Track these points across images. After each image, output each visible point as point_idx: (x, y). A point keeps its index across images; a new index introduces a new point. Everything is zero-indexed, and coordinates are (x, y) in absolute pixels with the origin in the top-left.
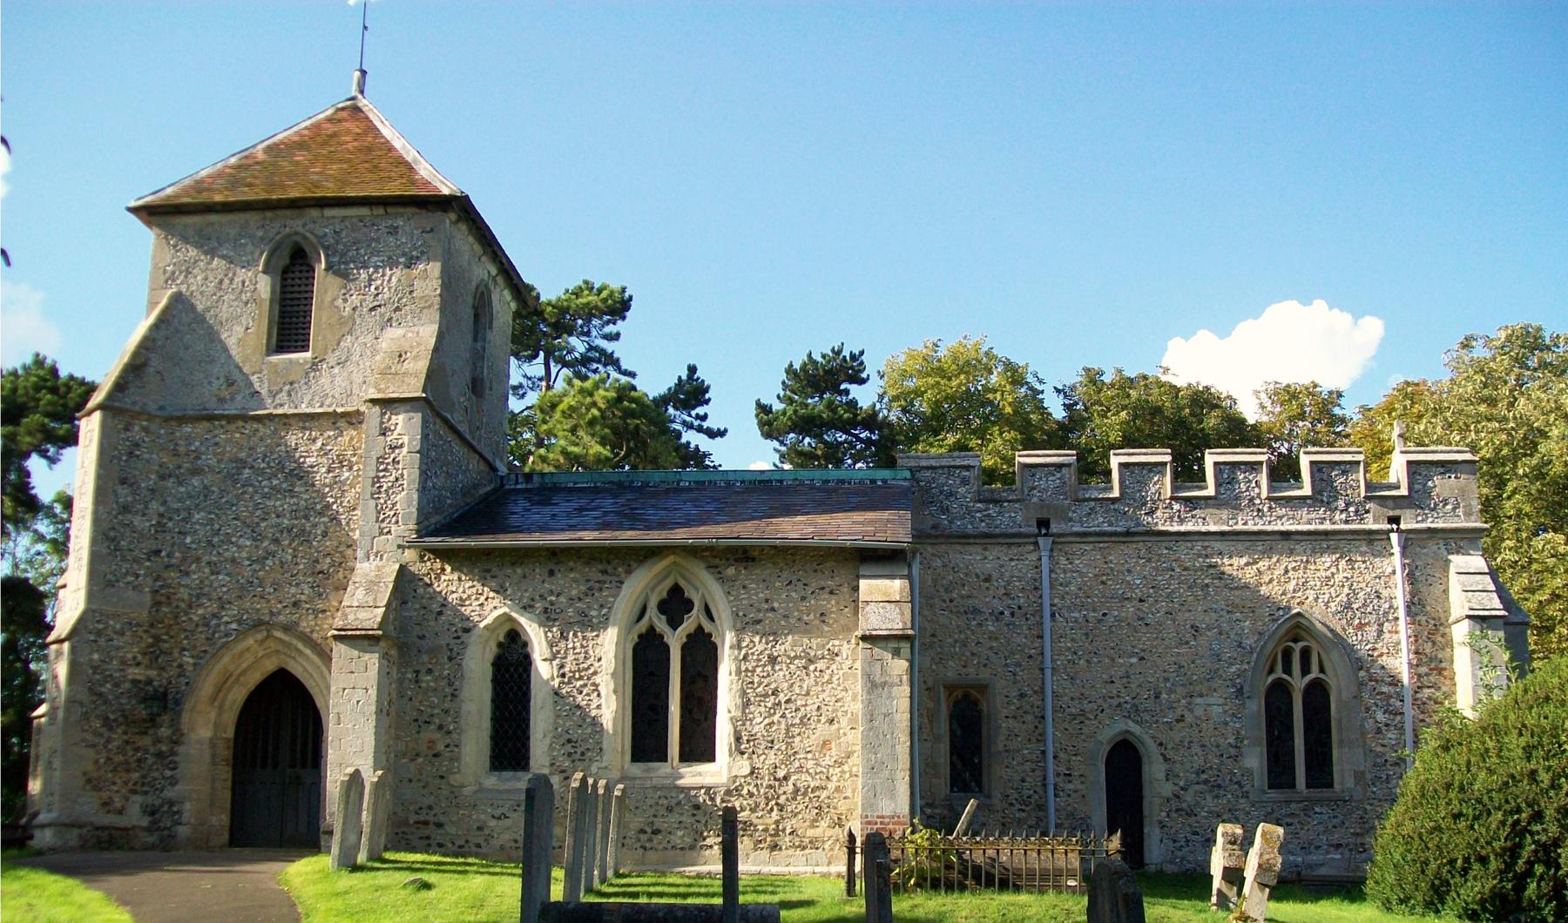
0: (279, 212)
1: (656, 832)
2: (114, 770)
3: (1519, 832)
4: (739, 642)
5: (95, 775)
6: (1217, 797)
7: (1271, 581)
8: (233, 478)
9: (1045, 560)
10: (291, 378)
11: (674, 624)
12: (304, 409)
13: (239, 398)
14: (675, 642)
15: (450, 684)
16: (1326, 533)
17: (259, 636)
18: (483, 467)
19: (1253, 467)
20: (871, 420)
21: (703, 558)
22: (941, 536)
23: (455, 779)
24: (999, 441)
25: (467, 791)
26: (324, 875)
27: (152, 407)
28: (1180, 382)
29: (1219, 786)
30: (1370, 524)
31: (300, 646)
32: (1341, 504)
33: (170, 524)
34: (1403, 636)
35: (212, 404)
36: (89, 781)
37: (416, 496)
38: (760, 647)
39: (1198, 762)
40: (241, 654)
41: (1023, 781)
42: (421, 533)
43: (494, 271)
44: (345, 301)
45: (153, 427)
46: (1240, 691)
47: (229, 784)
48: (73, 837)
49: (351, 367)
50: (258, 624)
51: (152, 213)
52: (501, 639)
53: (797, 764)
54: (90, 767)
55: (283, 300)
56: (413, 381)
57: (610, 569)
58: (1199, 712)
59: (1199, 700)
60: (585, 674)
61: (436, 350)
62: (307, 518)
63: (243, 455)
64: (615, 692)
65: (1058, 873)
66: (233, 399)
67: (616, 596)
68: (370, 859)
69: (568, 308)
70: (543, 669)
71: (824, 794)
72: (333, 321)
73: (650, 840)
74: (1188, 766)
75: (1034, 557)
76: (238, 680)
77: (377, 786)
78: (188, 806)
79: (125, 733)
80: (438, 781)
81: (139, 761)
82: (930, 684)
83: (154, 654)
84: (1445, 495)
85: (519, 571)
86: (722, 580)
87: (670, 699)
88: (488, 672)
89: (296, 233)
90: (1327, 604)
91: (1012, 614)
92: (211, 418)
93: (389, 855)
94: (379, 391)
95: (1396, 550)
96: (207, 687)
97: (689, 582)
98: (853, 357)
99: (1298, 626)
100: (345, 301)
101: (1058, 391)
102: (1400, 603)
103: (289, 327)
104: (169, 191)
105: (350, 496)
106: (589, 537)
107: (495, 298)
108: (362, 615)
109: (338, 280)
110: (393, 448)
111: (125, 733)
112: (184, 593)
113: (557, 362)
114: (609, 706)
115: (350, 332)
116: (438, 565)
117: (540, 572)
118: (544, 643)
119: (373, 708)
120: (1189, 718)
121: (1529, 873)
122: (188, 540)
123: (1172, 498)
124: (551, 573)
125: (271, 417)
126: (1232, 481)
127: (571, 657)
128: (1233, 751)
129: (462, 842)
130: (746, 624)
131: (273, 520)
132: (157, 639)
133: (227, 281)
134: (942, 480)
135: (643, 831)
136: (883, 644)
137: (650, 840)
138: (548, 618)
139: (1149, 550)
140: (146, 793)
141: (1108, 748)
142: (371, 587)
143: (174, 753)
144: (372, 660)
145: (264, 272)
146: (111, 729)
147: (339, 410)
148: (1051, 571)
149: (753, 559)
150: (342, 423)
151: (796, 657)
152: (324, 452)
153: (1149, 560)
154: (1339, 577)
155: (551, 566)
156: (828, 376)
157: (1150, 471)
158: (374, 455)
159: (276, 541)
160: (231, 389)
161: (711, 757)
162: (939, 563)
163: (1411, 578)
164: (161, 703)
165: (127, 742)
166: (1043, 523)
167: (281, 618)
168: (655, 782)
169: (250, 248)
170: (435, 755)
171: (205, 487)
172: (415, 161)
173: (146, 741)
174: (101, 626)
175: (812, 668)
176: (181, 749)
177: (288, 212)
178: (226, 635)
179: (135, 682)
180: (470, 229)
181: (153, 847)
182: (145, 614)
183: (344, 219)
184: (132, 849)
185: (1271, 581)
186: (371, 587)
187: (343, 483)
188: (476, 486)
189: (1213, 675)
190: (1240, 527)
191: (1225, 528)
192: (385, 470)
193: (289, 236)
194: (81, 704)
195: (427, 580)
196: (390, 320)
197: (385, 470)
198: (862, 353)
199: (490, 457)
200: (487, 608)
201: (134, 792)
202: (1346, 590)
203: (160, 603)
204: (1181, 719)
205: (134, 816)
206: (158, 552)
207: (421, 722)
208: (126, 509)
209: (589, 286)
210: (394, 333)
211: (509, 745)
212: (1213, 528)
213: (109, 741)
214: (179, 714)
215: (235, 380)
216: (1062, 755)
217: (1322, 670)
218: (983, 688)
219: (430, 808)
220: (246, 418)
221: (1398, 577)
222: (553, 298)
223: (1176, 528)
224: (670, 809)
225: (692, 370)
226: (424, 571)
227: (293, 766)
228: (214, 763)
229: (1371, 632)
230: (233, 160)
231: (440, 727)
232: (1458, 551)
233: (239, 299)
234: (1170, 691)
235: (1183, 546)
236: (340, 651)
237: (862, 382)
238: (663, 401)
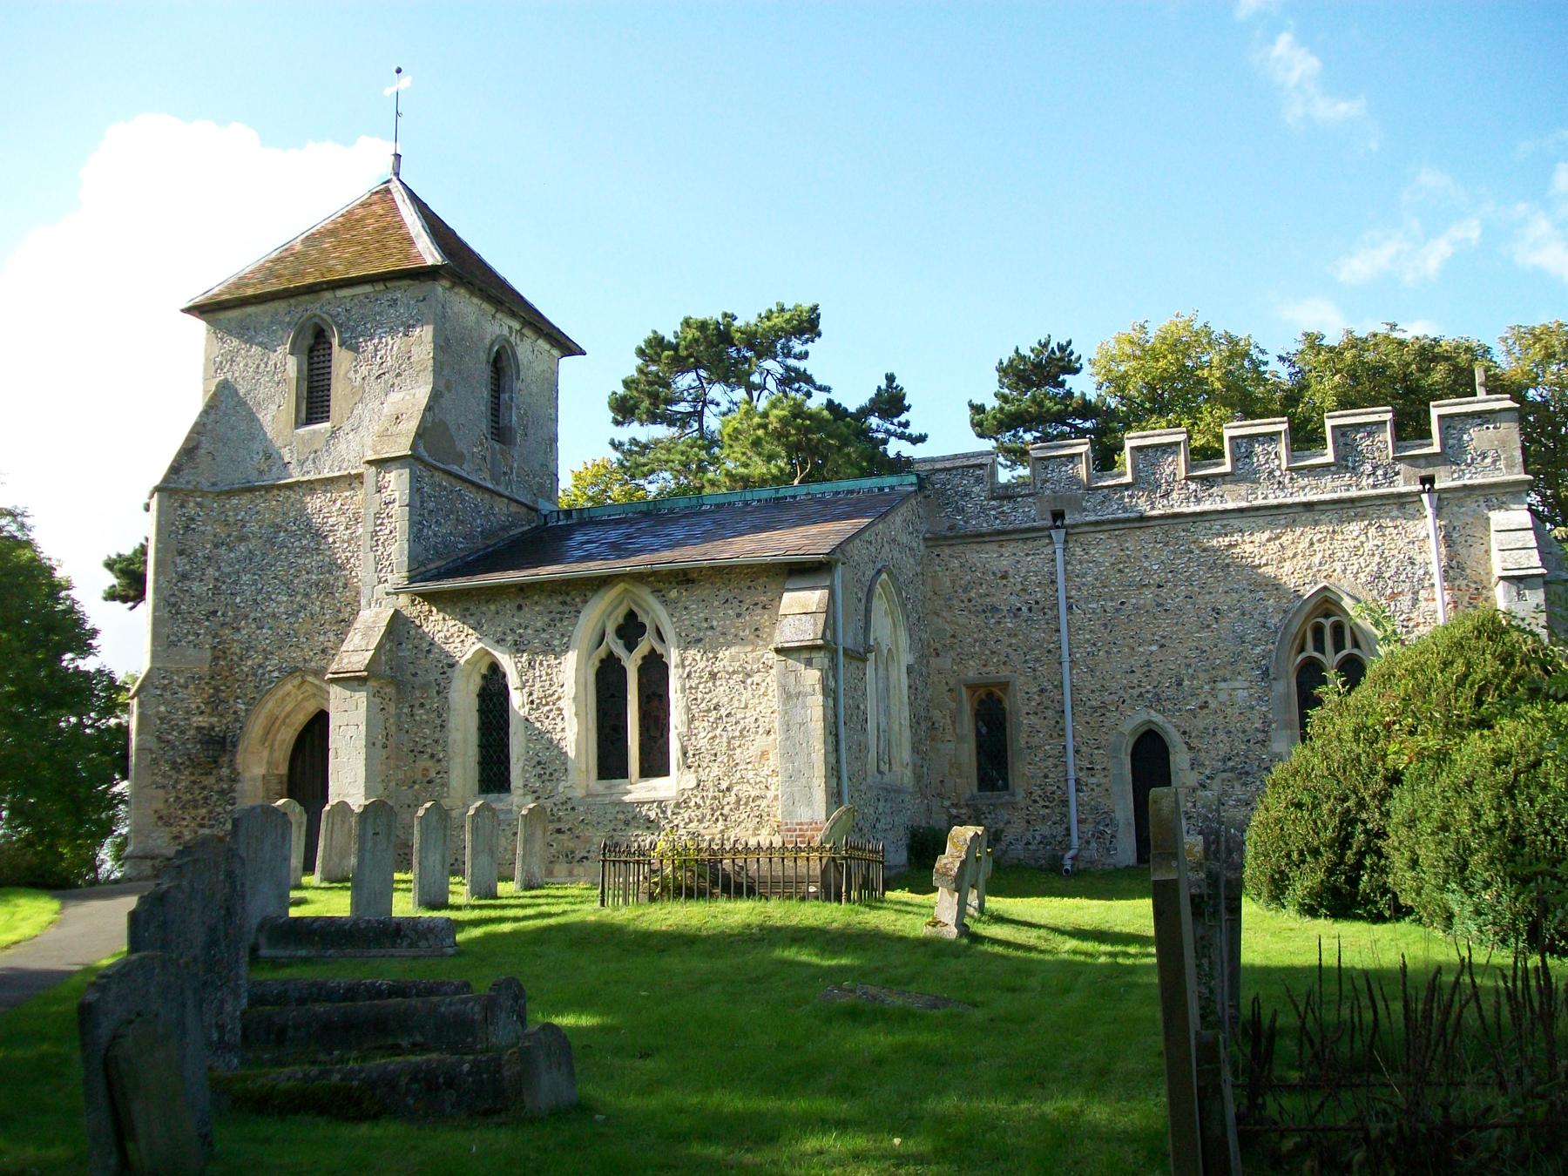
2: (183, 807)
3: (1348, 820)
4: (683, 660)
6: (1245, 784)
7: (1295, 555)
8: (270, 541)
9: (1059, 553)
12: (326, 474)
16: (1352, 500)
17: (296, 682)
19: (1272, 437)
20: (1086, 409)
21: (648, 583)
22: (956, 537)
24: (1209, 419)
27: (205, 485)
28: (1408, 337)
29: (1247, 773)
30: (1400, 487)
32: (1368, 468)
34: (1439, 604)
35: (254, 476)
36: (160, 818)
38: (702, 665)
39: (1224, 749)
40: (283, 699)
41: (1046, 777)
42: (412, 580)
44: (356, 372)
45: (207, 502)
46: (1266, 673)
49: (362, 431)
52: (484, 671)
53: (738, 775)
54: (160, 805)
57: (568, 599)
58: (1223, 697)
59: (1222, 685)
62: (330, 572)
63: (278, 520)
65: (799, 881)
70: (517, 699)
71: (764, 803)
74: (1213, 754)
75: (1049, 550)
79: (192, 774)
81: (206, 798)
82: (951, 686)
83: (215, 703)
84: (1485, 447)
85: (493, 607)
86: (665, 603)
87: (631, 717)
88: (474, 703)
90: (1356, 576)
91: (1030, 610)
92: (252, 490)
94: (376, 452)
95: (1429, 512)
96: (256, 729)
98: (1061, 348)
99: (1326, 600)
100: (356, 372)
101: (1281, 358)
102: (1434, 569)
103: (315, 403)
104: (216, 291)
111: (192, 774)
112: (236, 648)
114: (572, 731)
115: (361, 401)
116: (426, 608)
117: (510, 606)
120: (1213, 704)
121: (1359, 865)
123: (1187, 478)
124: (520, 608)
126: (1249, 455)
127: (538, 685)
128: (1260, 736)
130: (687, 643)
132: (217, 689)
134: (956, 481)
136: (796, 656)
138: (518, 648)
139: (1166, 533)
140: (212, 826)
141: (1132, 741)
143: (233, 791)
144: (361, 698)
146: (179, 771)
148: (1067, 563)
149: (693, 581)
151: (734, 672)
153: (1166, 544)
154: (1368, 546)
156: (1040, 371)
157: (1164, 452)
158: (372, 511)
159: (307, 595)
161: (665, 772)
162: (956, 563)
163: (1449, 541)
164: (218, 747)
165: (194, 782)
166: (1058, 515)
170: (429, 782)
175: (749, 681)
176: (238, 786)
177: (307, 297)
179: (199, 729)
182: (206, 667)
185: (1295, 555)
189: (1237, 657)
190: (1260, 502)
191: (1244, 504)
193: (310, 318)
194: (151, 751)
198: (1069, 343)
200: (467, 644)
202: (1377, 559)
204: (1205, 706)
207: (417, 752)
208: (184, 577)
210: (395, 397)
211: (494, 775)
212: (1230, 505)
213: (176, 782)
214: (234, 754)
216: (1084, 749)
217: (1356, 644)
218: (1005, 686)
220: (280, 487)
221: (1432, 542)
223: (1193, 508)
224: (627, 823)
225: (890, 378)
229: (1405, 601)
230: (274, 255)
231: (432, 756)
232: (1501, 506)
233: (273, 375)
234: (1193, 677)
235: (1201, 526)
236: (335, 690)
237: (1076, 371)
238: (864, 412)
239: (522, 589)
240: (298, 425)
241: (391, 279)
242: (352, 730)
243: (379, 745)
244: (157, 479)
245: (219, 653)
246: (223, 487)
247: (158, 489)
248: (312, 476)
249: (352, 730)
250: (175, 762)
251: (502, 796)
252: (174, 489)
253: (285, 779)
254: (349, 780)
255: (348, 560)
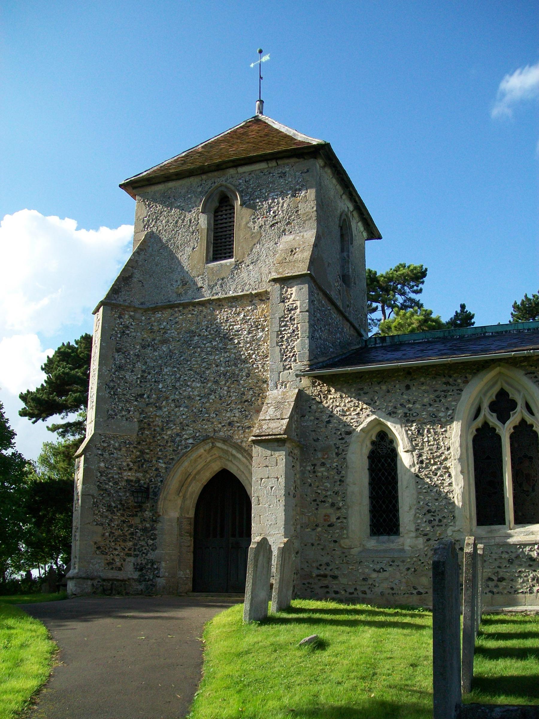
0: (210, 175)
1: (501, 580)
2: (115, 541)
5: (103, 544)
10: (222, 276)
11: (503, 419)
12: (231, 294)
13: (190, 292)
14: (505, 432)
15: (339, 473)
17: (207, 447)
18: (352, 332)
21: (521, 367)
23: (345, 543)
25: (354, 551)
26: (237, 631)
27: (137, 304)
31: (234, 452)
33: (149, 377)
36: (99, 548)
37: (307, 341)
40: (196, 461)
42: (312, 367)
43: (351, 208)
44: (254, 222)
45: (137, 316)
47: (192, 549)
48: (88, 586)
49: (259, 264)
50: (206, 439)
51: (134, 187)
52: (374, 438)
54: (99, 539)
55: (215, 229)
56: (301, 265)
57: (451, 380)
60: (438, 460)
61: (315, 245)
62: (235, 365)
63: (193, 328)
64: (462, 472)
66: (186, 293)
67: (457, 401)
68: (280, 609)
69: (393, 277)
70: (406, 459)
72: (248, 236)
73: (496, 586)
76: (194, 477)
77: (283, 551)
78: (163, 564)
79: (123, 515)
80: (332, 545)
81: (132, 534)
83: (141, 463)
85: (384, 388)
89: (221, 186)
92: (172, 306)
93: (296, 603)
94: (279, 273)
96: (174, 483)
97: (512, 386)
100: (254, 222)
103: (221, 244)
105: (264, 348)
106: (435, 360)
107: (353, 225)
108: (273, 425)
109: (250, 211)
110: (290, 310)
111: (123, 515)
112: (159, 421)
113: (388, 306)
114: (458, 486)
115: (259, 242)
116: (326, 388)
117: (399, 387)
118: (406, 439)
119: (283, 492)
122: (160, 386)
124: (408, 387)
125: (210, 301)
127: (426, 449)
129: (352, 590)
131: (214, 368)
133: (180, 221)
135: (490, 579)
137: (496, 586)
138: (407, 419)
140: (137, 556)
142: (279, 405)
143: (155, 529)
144: (281, 456)
145: (202, 212)
146: (113, 513)
147: (253, 292)
150: (256, 301)
152: (245, 321)
155: (407, 382)
158: (277, 316)
159: (216, 382)
160: (185, 288)
164: (144, 495)
165: (124, 522)
167: (221, 434)
168: (497, 540)
169: (194, 199)
170: (329, 526)
171: (170, 351)
172: (294, 134)
173: (136, 521)
174: (105, 445)
176: (159, 526)
177: (216, 174)
178: (186, 448)
179: (127, 481)
180: (333, 174)
181: (141, 593)
182: (134, 436)
183: (250, 173)
184: (127, 594)
186: (279, 405)
187: (259, 340)
188: (349, 344)
192: (285, 325)
193: (217, 188)
194: (93, 497)
195: (318, 399)
196: (284, 231)
197: (285, 325)
199: (357, 326)
200: (363, 416)
201: (129, 555)
203: (144, 429)
205: (129, 572)
206: (142, 396)
208: (120, 368)
209: (404, 266)
210: (287, 239)
215: (186, 282)
219: (328, 564)
220: (195, 305)
222: (384, 274)
224: (511, 561)
225: (463, 307)
226: (316, 393)
227: (234, 535)
228: (181, 535)
231: (333, 505)
233: (188, 231)
236: (257, 450)
239: (409, 372)
240: (208, 261)
241: (281, 158)
242: (272, 482)
243: (292, 494)
244: (102, 295)
245: (145, 425)
246: (148, 305)
247: (102, 303)
248: (220, 296)
249: (272, 482)
250: (110, 506)
251: (392, 537)
252: (115, 303)
253: (193, 520)
254: (269, 522)
255: (250, 355)
